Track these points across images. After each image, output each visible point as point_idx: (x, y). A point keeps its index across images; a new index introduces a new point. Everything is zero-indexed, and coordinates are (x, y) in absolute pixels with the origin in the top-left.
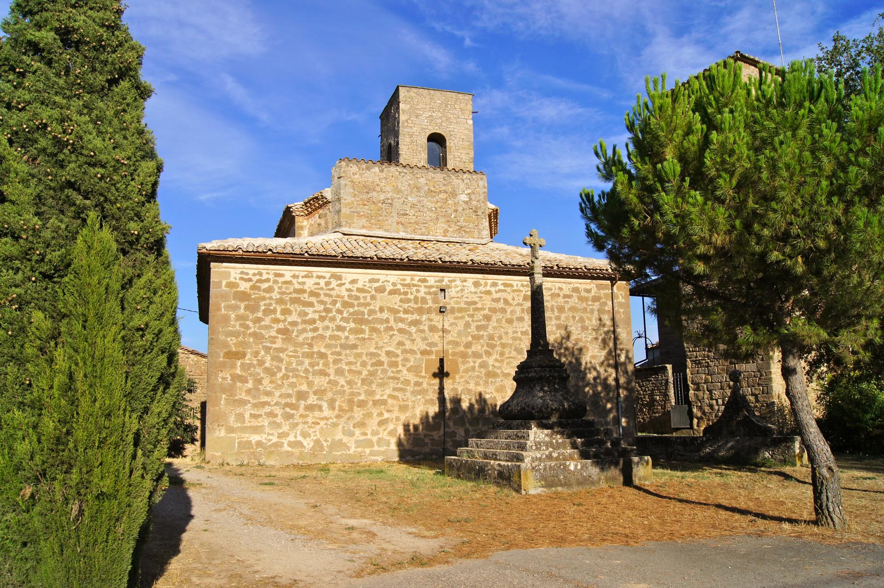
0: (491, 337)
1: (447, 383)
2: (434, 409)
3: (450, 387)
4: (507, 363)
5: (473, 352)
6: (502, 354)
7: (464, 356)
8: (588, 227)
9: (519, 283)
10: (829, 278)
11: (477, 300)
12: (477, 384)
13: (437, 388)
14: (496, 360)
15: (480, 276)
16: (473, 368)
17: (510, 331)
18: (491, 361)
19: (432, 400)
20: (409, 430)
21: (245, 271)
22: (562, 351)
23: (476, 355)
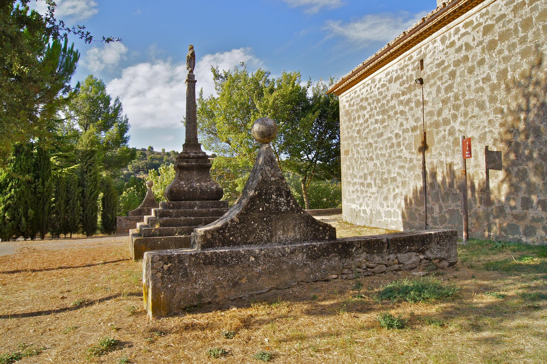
0: (456, 98)
1: (427, 155)
2: (420, 184)
3: (431, 158)
4: (471, 125)
5: (443, 119)
6: (466, 114)
7: (437, 125)
8: (316, 5)
9: (478, 15)
10: (205, 326)
11: (444, 57)
12: (447, 155)
13: (421, 163)
14: (462, 124)
15: (444, 29)
16: (444, 137)
17: (472, 83)
18: (457, 126)
19: (418, 175)
20: (417, 196)
21: (468, 20)
22: (531, 89)
23: (446, 122)
